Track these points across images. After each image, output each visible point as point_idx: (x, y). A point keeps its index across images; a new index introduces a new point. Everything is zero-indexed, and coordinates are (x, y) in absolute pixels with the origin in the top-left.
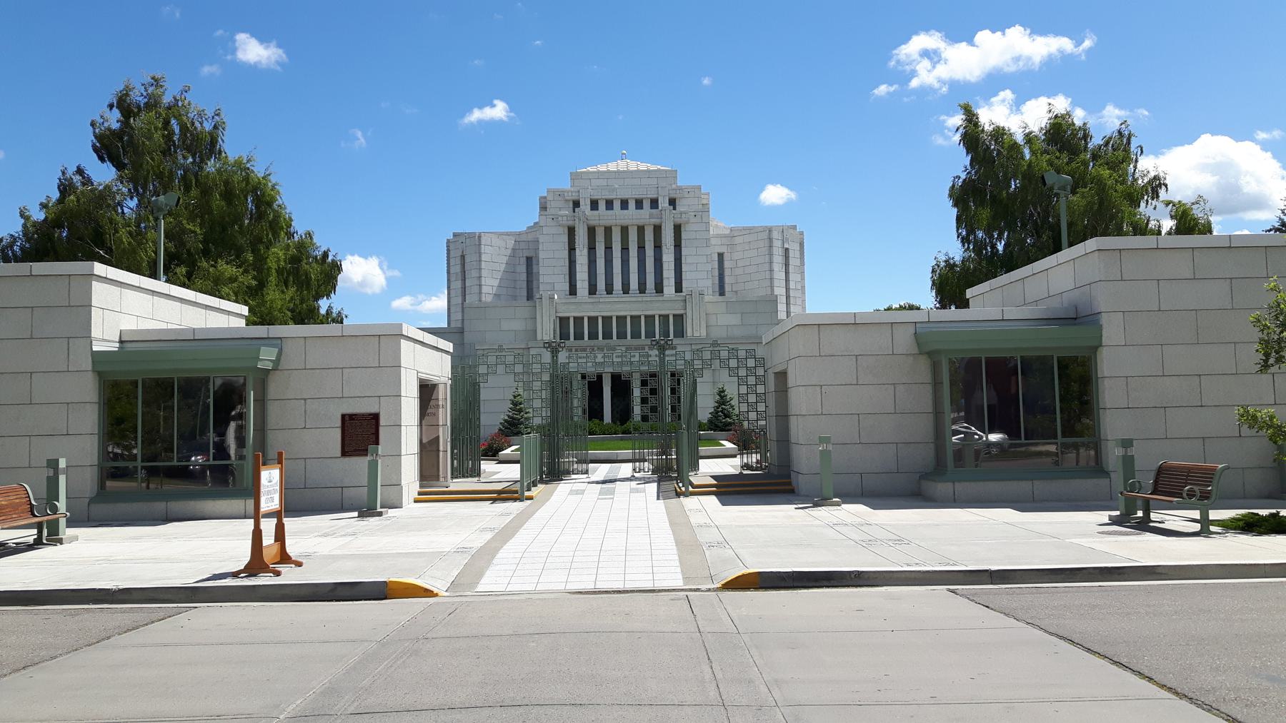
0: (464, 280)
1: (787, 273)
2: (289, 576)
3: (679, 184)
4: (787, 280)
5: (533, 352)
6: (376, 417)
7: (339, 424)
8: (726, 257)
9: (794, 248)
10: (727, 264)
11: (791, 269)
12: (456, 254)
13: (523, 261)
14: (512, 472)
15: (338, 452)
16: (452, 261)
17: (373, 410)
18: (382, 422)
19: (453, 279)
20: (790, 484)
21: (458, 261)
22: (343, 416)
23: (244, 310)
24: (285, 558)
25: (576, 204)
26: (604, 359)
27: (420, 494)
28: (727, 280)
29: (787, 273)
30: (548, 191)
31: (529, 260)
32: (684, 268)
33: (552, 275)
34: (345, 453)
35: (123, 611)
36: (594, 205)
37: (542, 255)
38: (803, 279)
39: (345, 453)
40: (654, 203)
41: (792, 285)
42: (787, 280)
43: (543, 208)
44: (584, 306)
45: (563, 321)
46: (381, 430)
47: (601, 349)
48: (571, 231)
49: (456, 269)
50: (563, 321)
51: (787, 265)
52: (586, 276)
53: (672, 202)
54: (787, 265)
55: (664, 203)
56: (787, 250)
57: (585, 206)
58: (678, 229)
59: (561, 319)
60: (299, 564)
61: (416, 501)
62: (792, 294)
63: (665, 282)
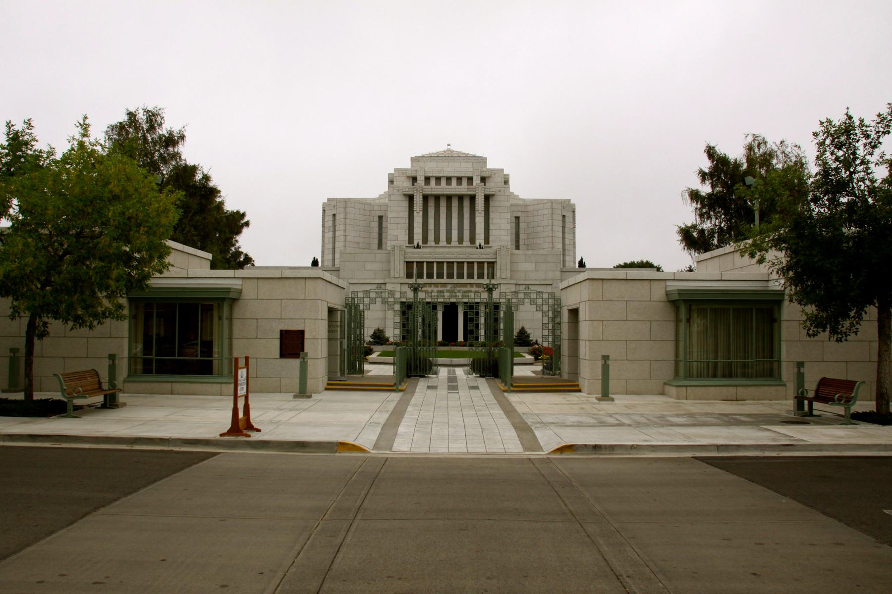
0: (334, 231)
1: (564, 233)
2: (255, 437)
3: (488, 167)
4: (564, 238)
5: (389, 287)
6: (302, 333)
7: (278, 336)
8: (521, 219)
9: (569, 215)
10: (522, 225)
11: (567, 230)
12: (329, 213)
13: (376, 219)
14: (388, 371)
15: (278, 356)
16: (327, 218)
17: (300, 328)
18: (307, 336)
19: (327, 230)
20: (578, 385)
21: (331, 218)
22: (281, 331)
23: (210, 256)
24: (250, 427)
25: (414, 179)
26: (437, 292)
27: (328, 384)
28: (522, 236)
29: (564, 233)
30: (395, 170)
31: (380, 218)
32: (491, 227)
33: (396, 232)
34: (283, 355)
35: (820, 447)
36: (427, 179)
37: (390, 215)
38: (574, 237)
39: (283, 355)
40: (470, 179)
41: (567, 242)
42: (564, 238)
43: (391, 182)
44: (486, 277)
45: (409, 264)
46: (306, 341)
47: (436, 285)
48: (411, 198)
49: (329, 224)
50: (409, 264)
51: (564, 227)
52: (420, 231)
53: (483, 179)
54: (564, 227)
55: (477, 181)
56: (564, 216)
57: (421, 181)
58: (487, 198)
59: (407, 262)
60: (259, 430)
61: (326, 389)
62: (567, 248)
63: (477, 237)
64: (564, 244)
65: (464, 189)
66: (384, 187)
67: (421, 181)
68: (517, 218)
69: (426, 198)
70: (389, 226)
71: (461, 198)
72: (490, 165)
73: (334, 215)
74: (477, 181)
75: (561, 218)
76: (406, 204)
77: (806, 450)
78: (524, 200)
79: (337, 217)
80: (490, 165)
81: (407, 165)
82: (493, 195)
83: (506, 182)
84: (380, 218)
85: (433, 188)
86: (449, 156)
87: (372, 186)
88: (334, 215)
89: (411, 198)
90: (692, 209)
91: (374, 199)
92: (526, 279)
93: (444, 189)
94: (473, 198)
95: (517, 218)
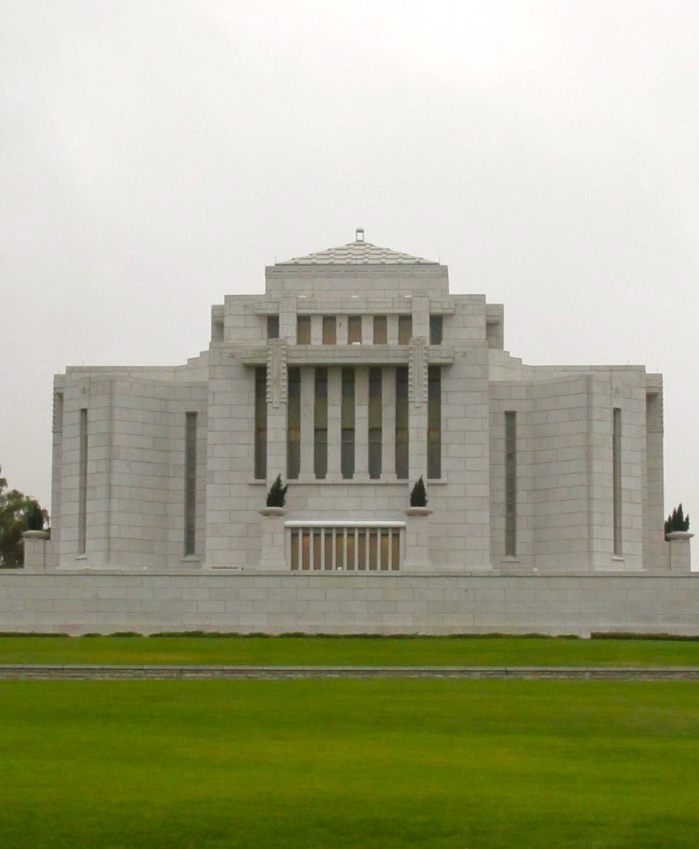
3: (453, 290)
8: (520, 419)
13: (182, 420)
21: (76, 417)
30: (228, 298)
31: (191, 416)
36: (303, 321)
37: (212, 411)
43: (219, 326)
48: (260, 373)
53: (437, 322)
57: (288, 328)
58: (435, 373)
64: (84, 474)
65: (391, 351)
66: (198, 340)
67: (288, 328)
68: (510, 415)
69: (294, 373)
70: (211, 438)
71: (375, 372)
72: (458, 285)
73: (84, 411)
74: (421, 329)
75: (609, 415)
76: (250, 385)
77: (376, 555)
78: (535, 369)
79: (91, 415)
80: (458, 285)
81: (256, 286)
82: (448, 366)
83: (494, 326)
84: (191, 416)
85: (317, 351)
86: (358, 265)
87: (169, 335)
88: (84, 411)
89: (260, 373)
90: (25, 495)
91: (176, 370)
92: (589, 573)
93: (343, 350)
94: (401, 372)
95: (510, 415)
